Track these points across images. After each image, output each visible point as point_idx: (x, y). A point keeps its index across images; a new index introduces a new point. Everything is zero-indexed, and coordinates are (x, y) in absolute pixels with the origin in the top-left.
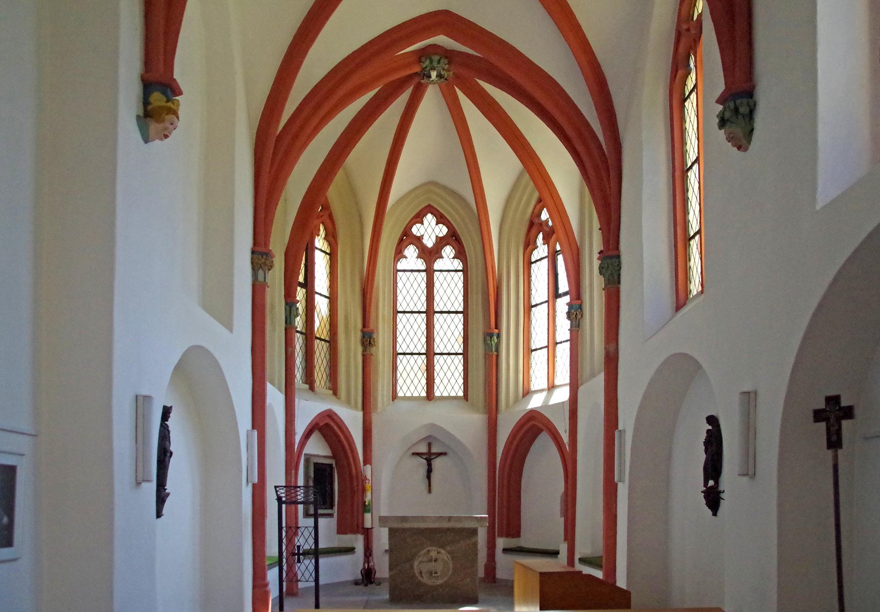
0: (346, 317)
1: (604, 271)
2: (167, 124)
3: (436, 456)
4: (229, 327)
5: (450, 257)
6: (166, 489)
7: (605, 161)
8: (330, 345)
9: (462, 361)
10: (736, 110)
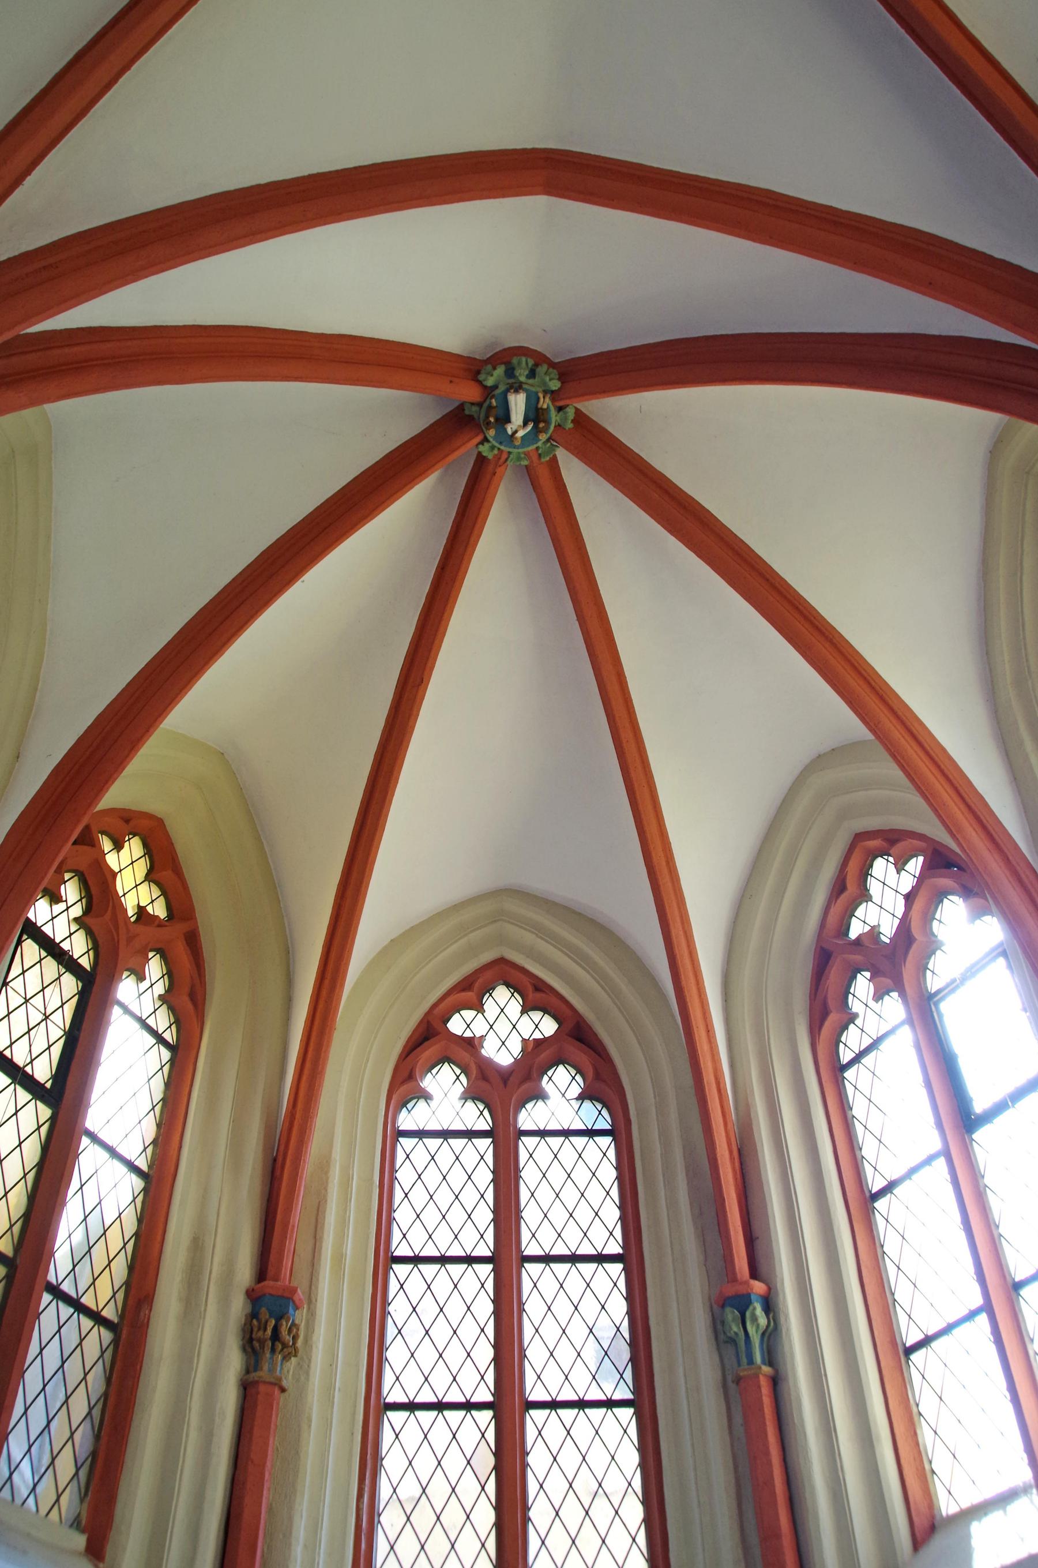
0: (197, 1245)
5: (568, 1095)
8: (116, 1342)
9: (633, 1430)
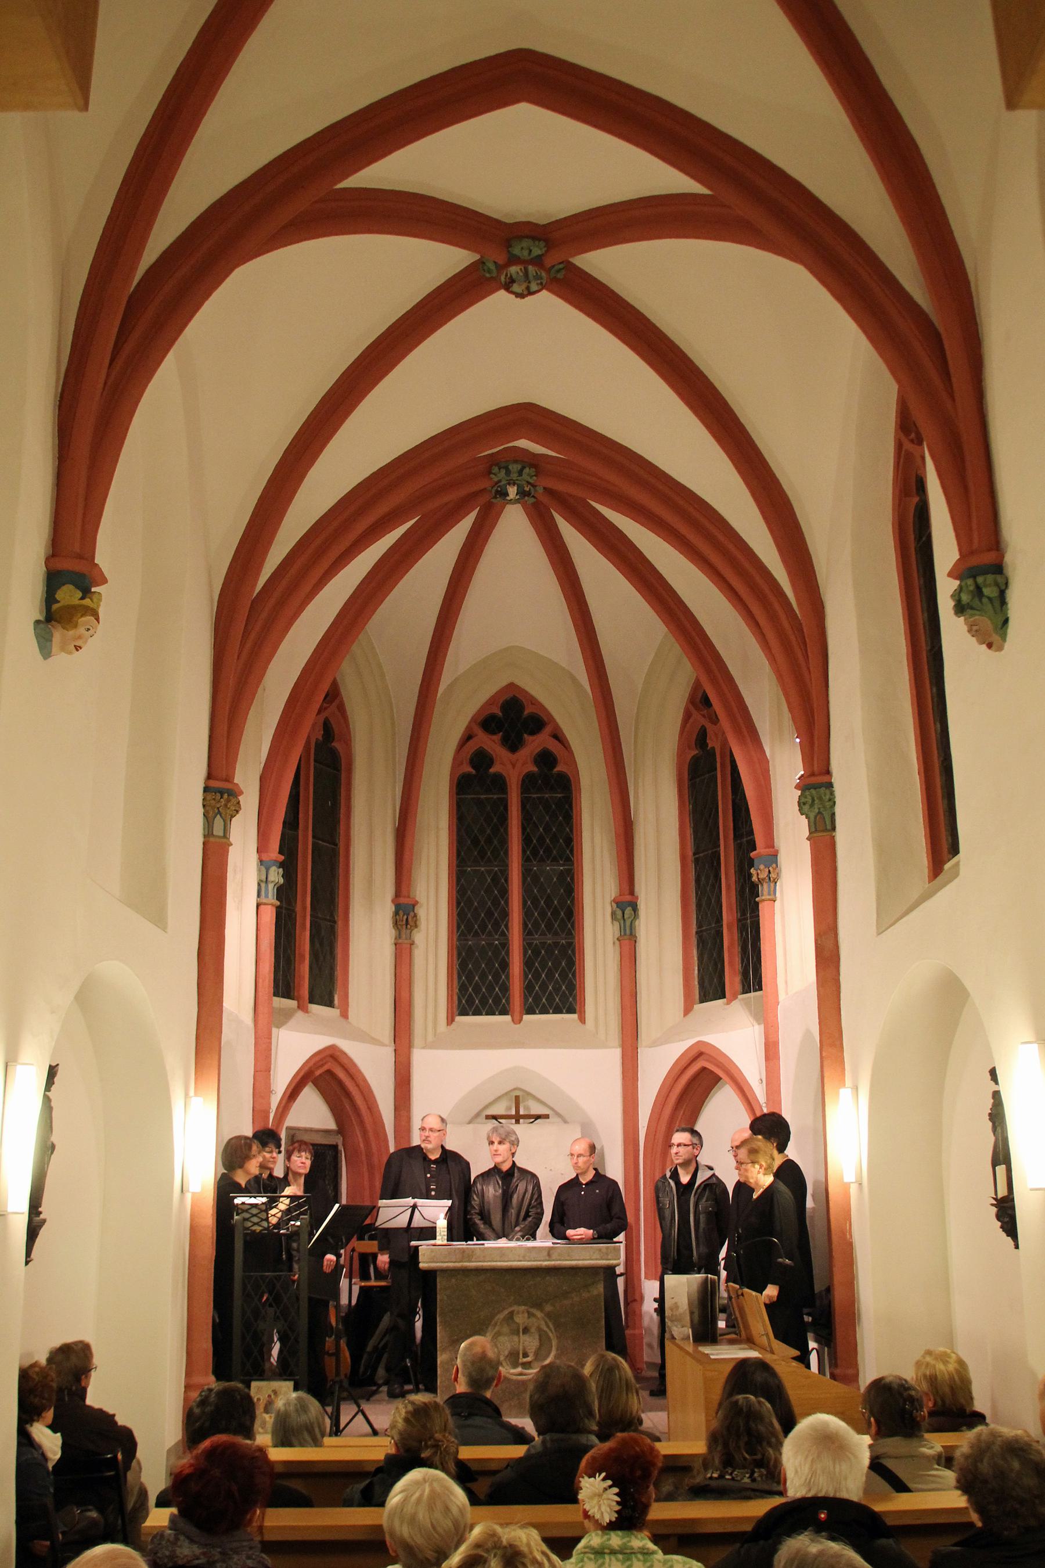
1: (806, 808)
2: (81, 630)
3: (533, 1120)
4: (159, 920)
6: (41, 1213)
7: (799, 628)
10: (979, 591)
